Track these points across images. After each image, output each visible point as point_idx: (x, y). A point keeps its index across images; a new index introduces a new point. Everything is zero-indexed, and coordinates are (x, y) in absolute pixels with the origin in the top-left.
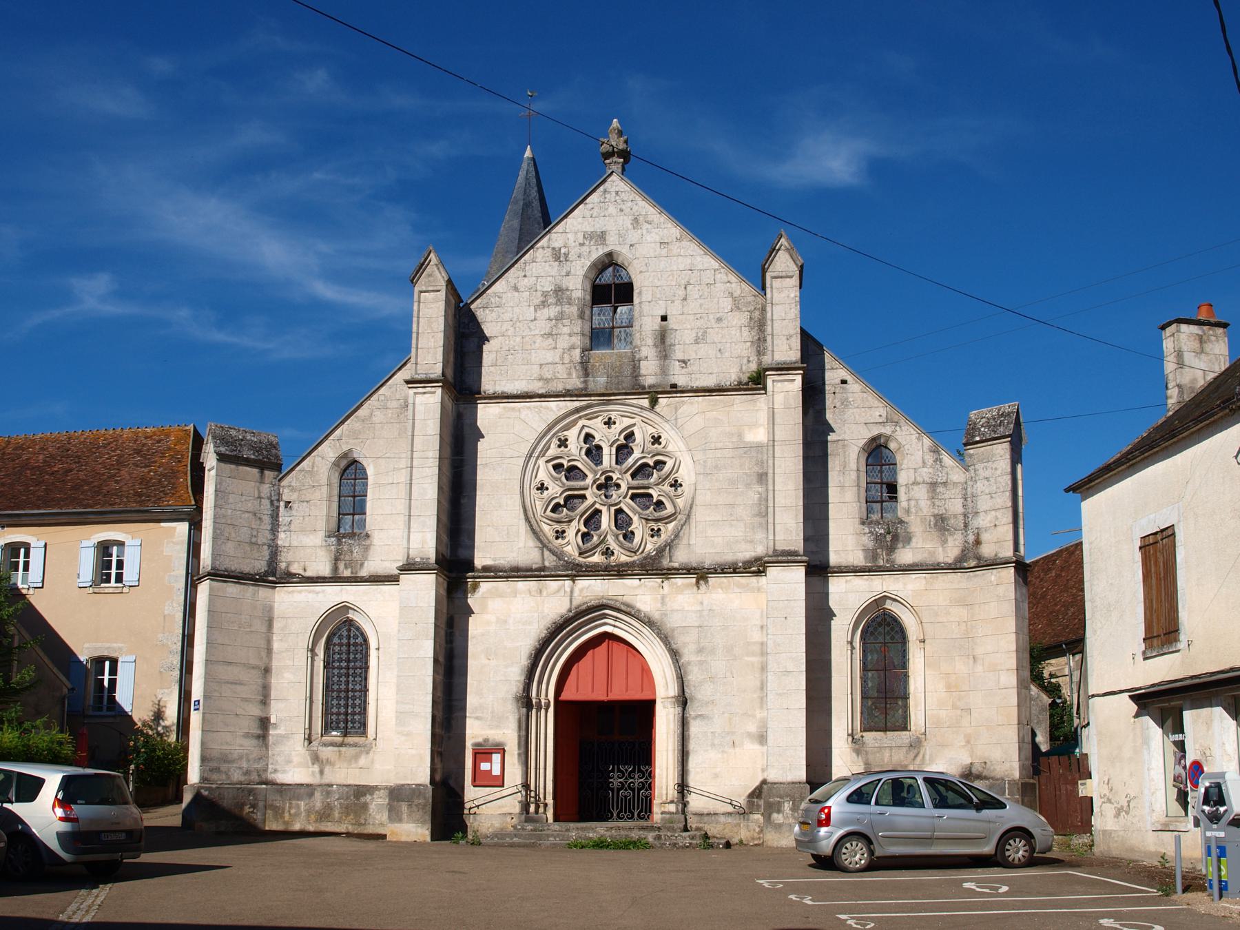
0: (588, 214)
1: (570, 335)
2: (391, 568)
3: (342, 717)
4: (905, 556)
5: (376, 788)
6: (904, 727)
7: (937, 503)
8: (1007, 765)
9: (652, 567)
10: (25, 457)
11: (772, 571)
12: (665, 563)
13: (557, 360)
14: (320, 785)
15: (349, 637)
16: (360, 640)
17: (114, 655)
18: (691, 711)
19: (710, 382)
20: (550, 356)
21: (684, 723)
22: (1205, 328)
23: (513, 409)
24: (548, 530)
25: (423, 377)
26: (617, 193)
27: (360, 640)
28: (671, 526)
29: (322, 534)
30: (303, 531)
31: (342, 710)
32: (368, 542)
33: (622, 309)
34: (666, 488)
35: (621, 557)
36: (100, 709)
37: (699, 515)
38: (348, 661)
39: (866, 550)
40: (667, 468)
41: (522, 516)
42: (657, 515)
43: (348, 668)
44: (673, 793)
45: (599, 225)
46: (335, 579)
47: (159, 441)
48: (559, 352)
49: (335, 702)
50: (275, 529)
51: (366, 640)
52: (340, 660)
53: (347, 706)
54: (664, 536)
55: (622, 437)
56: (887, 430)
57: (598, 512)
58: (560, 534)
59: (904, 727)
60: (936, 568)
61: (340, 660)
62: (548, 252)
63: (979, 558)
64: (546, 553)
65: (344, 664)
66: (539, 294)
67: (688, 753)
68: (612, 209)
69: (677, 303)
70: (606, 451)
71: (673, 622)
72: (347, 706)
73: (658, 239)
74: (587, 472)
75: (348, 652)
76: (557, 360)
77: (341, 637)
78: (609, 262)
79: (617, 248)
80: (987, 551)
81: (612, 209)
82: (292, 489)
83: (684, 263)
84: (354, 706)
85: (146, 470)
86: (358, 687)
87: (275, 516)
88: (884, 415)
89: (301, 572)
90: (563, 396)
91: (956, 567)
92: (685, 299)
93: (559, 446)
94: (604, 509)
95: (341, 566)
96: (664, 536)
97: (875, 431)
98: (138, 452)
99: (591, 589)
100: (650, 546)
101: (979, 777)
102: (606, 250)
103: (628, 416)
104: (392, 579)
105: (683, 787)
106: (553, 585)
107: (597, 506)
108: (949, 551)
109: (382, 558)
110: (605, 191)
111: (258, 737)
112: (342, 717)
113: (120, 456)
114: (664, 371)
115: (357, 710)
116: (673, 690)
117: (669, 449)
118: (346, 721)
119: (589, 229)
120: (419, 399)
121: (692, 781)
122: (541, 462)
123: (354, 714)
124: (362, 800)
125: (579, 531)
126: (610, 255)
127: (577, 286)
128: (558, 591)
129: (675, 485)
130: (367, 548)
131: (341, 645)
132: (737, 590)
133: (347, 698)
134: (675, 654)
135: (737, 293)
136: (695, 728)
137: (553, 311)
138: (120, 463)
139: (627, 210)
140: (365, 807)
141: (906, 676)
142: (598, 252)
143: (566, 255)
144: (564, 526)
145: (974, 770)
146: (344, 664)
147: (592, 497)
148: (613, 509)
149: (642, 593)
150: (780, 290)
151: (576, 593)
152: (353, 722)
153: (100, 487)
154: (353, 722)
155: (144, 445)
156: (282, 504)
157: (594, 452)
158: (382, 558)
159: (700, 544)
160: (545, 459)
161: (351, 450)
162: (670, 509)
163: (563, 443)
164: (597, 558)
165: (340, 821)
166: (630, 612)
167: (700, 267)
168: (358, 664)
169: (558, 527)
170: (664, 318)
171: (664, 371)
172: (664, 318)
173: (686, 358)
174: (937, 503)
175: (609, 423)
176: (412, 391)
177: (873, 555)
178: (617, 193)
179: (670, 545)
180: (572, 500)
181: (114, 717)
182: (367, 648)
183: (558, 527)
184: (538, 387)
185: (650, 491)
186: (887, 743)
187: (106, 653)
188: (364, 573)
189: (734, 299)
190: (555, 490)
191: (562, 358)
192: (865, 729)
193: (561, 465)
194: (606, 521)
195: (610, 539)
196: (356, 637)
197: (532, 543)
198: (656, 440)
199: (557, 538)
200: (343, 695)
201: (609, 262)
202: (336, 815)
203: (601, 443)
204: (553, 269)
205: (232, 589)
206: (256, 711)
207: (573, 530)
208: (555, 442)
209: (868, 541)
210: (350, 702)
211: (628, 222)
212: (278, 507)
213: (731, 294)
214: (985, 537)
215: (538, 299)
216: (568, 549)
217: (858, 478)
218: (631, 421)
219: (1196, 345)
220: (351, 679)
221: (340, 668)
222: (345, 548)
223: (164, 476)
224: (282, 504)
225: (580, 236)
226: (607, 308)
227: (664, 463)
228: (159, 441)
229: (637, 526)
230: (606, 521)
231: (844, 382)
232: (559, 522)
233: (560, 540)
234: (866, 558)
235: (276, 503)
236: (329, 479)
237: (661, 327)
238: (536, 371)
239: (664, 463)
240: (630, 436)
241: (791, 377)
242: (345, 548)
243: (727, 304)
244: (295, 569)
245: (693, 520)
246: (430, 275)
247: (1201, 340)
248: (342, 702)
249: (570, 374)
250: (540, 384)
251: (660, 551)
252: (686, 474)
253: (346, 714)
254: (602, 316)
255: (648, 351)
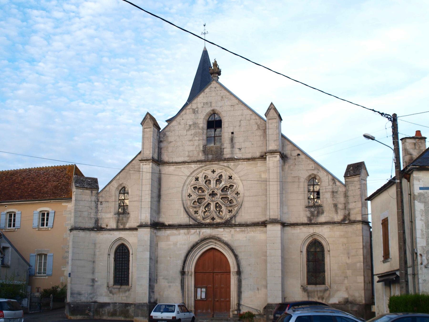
0: (205, 95)
1: (199, 140)
2: (141, 230)
3: (120, 278)
4: (322, 219)
5: (132, 304)
6: (323, 283)
7: (334, 199)
8: (360, 299)
9: (228, 224)
10: (14, 178)
11: (269, 227)
12: (233, 222)
13: (194, 149)
14: (112, 303)
15: (122, 250)
16: (126, 251)
17: (46, 253)
18: (243, 276)
19: (249, 156)
20: (191, 148)
21: (240, 282)
22: (417, 140)
23: (179, 168)
24: (192, 211)
25: (145, 158)
26: (215, 88)
27: (126, 251)
28: (236, 209)
29: (113, 213)
30: (106, 212)
31: (120, 276)
32: (128, 216)
33: (218, 130)
34: (234, 195)
35: (218, 220)
36: (41, 273)
37: (245, 204)
38: (122, 258)
39: (308, 217)
40: (234, 187)
41: (182, 206)
42: (230, 205)
43: (122, 261)
44: (236, 307)
45: (210, 99)
46: (117, 229)
47: (62, 171)
48: (194, 147)
49: (118, 273)
50: (97, 212)
51: (128, 251)
52: (120, 258)
53: (122, 274)
54: (234, 213)
55: (218, 176)
56: (315, 172)
57: (209, 204)
58: (196, 212)
59: (323, 283)
60: (334, 223)
61: (120, 258)
62: (191, 110)
63: (349, 220)
64: (191, 219)
65: (121, 259)
66: (188, 125)
67: (241, 292)
68: (213, 94)
69: (238, 127)
70: (212, 182)
71: (234, 245)
72: (122, 274)
73: (230, 104)
74: (205, 190)
75: (122, 255)
76: (194, 149)
77: (120, 250)
78: (214, 113)
79: (216, 108)
80: (352, 218)
81: (213, 94)
82: (102, 196)
83: (239, 113)
84: (124, 274)
85: (57, 183)
86: (126, 268)
87: (97, 207)
88: (314, 167)
89: (106, 227)
90: (197, 162)
91: (341, 223)
92: (240, 126)
93: (196, 180)
94: (211, 203)
95: (119, 224)
96: (234, 213)
97: (311, 172)
98: (55, 176)
99: (207, 232)
100: (228, 216)
101: (351, 303)
102: (213, 108)
103: (220, 168)
104: (135, 229)
105: (239, 305)
106: (192, 231)
107: (209, 202)
108: (339, 217)
109: (132, 223)
110: (211, 88)
111: (91, 286)
112: (120, 278)
113: (48, 178)
114: (232, 153)
115: (126, 276)
116: (236, 270)
117: (235, 181)
118: (122, 280)
119: (205, 101)
120: (144, 166)
121: (242, 302)
122: (189, 186)
123: (124, 277)
124: (127, 308)
125: (202, 211)
126: (213, 110)
127: (202, 123)
128: (195, 233)
129: (237, 194)
130: (128, 218)
131: (120, 253)
132: (259, 232)
133: (122, 272)
134: (236, 256)
135: (259, 123)
136: (243, 283)
137: (193, 132)
138: (48, 181)
139: (219, 94)
140: (128, 311)
141: (324, 264)
142: (208, 110)
143: (197, 111)
144: (197, 209)
145: (349, 300)
146: (121, 259)
147: (208, 199)
148: (215, 203)
149: (225, 234)
150: (271, 124)
151: (201, 233)
152: (124, 280)
153: (40, 190)
154: (124, 280)
155: (57, 173)
156: (99, 203)
157: (208, 181)
158: (132, 223)
159: (245, 216)
160: (191, 185)
161: (122, 183)
162: (235, 203)
163: (197, 179)
164: (208, 221)
165: (119, 316)
166: (219, 240)
167: (246, 114)
168: (126, 259)
169: (195, 210)
170: (232, 133)
171: (232, 153)
172: (232, 133)
173: (240, 147)
174: (334, 199)
175: (213, 172)
176: (141, 164)
177: (310, 219)
178: (215, 88)
179: (235, 216)
180: (200, 200)
181: (45, 276)
182: (129, 254)
183: (195, 210)
184: (186, 159)
185: (228, 196)
186: (316, 289)
187: (43, 253)
188: (127, 226)
189: (258, 125)
190: (195, 197)
191: (196, 148)
192: (309, 283)
193: (196, 187)
194: (212, 207)
195: (214, 213)
196: (125, 250)
197: (186, 215)
198: (230, 178)
199: (195, 214)
200: (120, 271)
201: (214, 113)
202: (118, 314)
203: (210, 179)
204: (193, 116)
205: (82, 234)
206: (90, 276)
207: (202, 209)
208: (194, 179)
209: (309, 214)
210: (123, 273)
211: (220, 98)
212: (98, 204)
213: (257, 123)
214: (352, 212)
215: (188, 127)
216: (199, 217)
217: (278, 199)
218: (221, 171)
219: (413, 146)
220: (123, 265)
221: (120, 261)
222: (121, 218)
223: (63, 185)
224: (99, 203)
225: (202, 104)
226: (213, 130)
227: (233, 186)
228: (62, 171)
229: (224, 208)
230: (212, 207)
231: (299, 155)
232: (195, 207)
233: (196, 214)
234: (308, 220)
235: (97, 203)
236: (115, 193)
237: (232, 136)
238: (187, 154)
239: (233, 186)
240: (221, 176)
241: (275, 156)
242: (121, 218)
243: (255, 127)
244: (104, 226)
245: (243, 207)
246: (147, 122)
247: (415, 144)
248: (120, 273)
249: (199, 154)
250: (188, 158)
251: (231, 218)
252: (241, 189)
253: (122, 277)
254: (212, 132)
255: (227, 145)
